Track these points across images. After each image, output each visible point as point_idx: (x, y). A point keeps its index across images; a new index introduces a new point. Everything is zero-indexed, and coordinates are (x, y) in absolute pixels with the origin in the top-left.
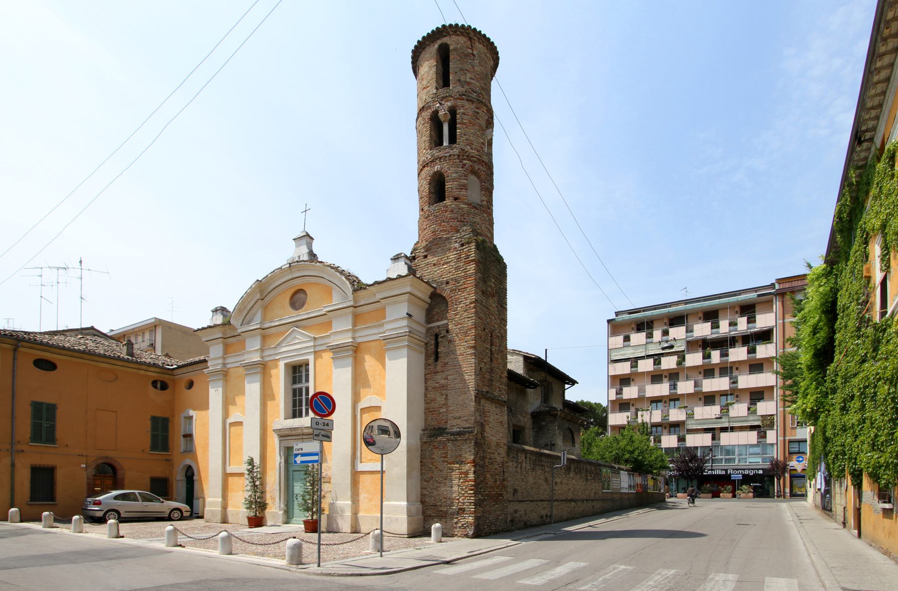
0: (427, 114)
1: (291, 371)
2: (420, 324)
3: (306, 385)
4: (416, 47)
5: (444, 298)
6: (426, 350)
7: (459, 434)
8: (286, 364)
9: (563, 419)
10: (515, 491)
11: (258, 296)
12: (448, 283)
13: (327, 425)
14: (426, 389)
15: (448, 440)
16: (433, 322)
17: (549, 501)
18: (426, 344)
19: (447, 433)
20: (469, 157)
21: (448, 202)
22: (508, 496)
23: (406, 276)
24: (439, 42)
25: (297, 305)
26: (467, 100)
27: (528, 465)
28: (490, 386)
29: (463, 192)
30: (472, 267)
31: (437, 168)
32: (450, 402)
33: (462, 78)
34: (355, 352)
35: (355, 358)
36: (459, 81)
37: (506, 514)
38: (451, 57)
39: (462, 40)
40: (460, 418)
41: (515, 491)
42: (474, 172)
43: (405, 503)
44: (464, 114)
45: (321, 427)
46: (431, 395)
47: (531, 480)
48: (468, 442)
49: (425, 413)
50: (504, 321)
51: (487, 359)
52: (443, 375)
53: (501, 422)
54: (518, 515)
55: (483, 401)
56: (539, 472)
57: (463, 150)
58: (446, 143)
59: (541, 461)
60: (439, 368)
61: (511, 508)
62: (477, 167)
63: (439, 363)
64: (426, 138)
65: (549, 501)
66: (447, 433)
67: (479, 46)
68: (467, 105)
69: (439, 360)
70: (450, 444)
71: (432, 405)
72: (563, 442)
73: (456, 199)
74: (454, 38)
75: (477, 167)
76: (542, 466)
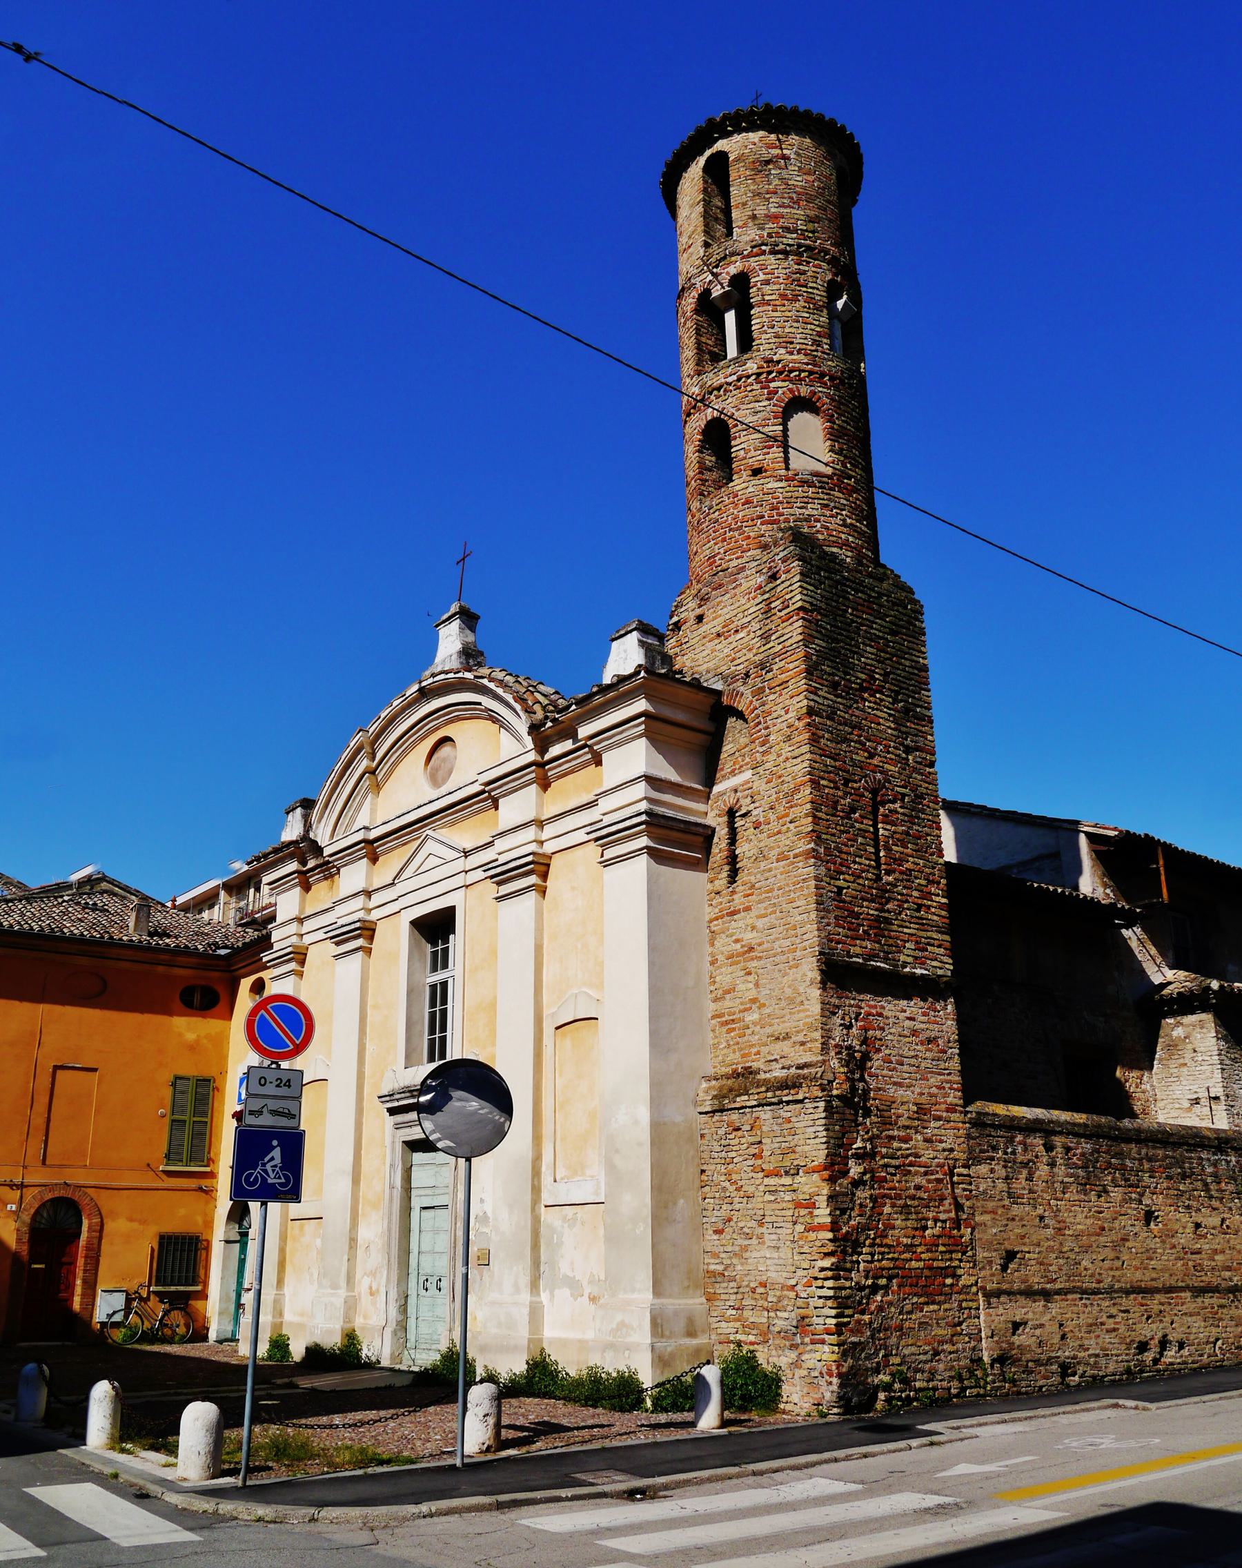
7: (785, 1085)
13: (288, 1084)
21: (741, 483)
24: (708, 153)
30: (794, 630)
38: (733, 174)
40: (787, 1037)
44: (767, 282)
45: (270, 1089)
57: (769, 361)
58: (732, 349)
63: (739, 887)
69: (742, 877)
70: (765, 1114)
73: (757, 472)
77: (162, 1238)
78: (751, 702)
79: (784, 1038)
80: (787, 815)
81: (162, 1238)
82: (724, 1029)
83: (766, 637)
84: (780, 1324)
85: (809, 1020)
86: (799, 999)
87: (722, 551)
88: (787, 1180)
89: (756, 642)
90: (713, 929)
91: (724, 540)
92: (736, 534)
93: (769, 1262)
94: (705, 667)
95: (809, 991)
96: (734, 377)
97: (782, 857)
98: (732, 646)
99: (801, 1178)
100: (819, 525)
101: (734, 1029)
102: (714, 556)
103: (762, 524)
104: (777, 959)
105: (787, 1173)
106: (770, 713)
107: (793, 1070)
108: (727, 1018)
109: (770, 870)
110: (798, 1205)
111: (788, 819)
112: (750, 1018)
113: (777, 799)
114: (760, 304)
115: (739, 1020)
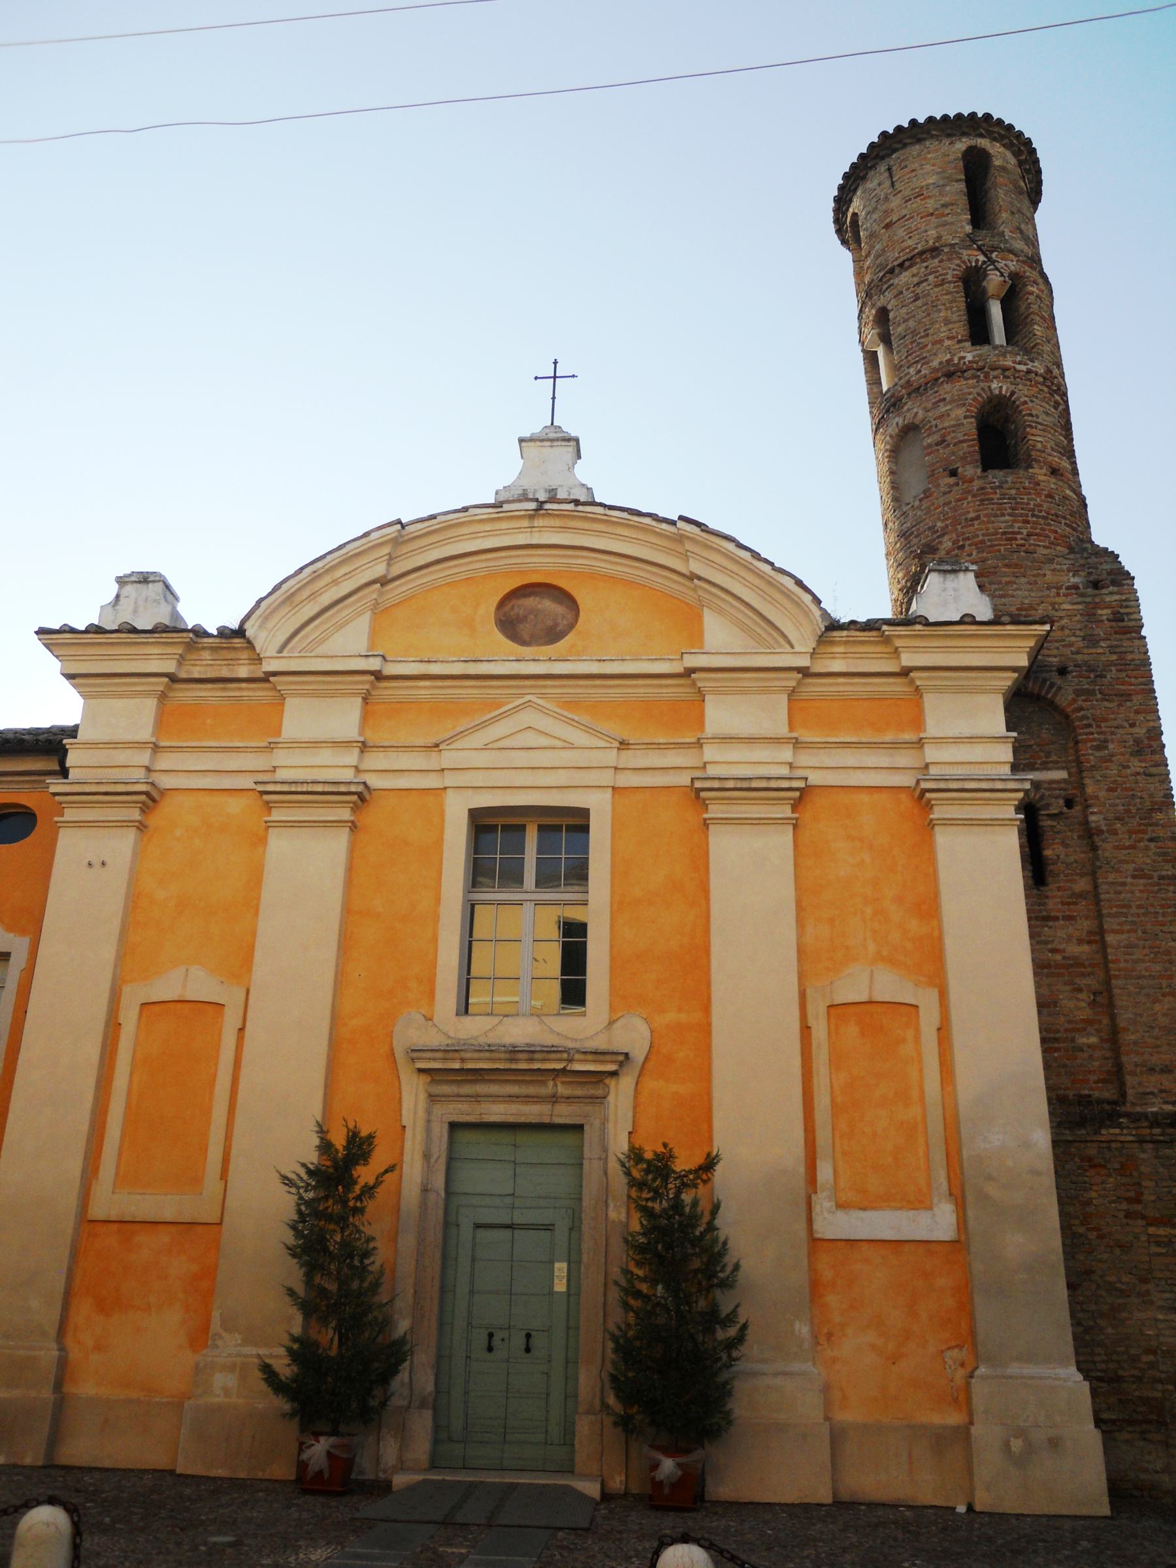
12: (1063, 671)
15: (1141, 1141)
25: (525, 629)
70: (1146, 1155)
77: (471, 811)
78: (1074, 701)
79: (1162, 1071)
81: (471, 811)
87: (1025, 532)
93: (1161, 1326)
97: (1139, 874)
101: (1057, 1050)
104: (1144, 982)
109: (1124, 884)
111: (1146, 837)
112: (1085, 1040)
113: (1128, 811)
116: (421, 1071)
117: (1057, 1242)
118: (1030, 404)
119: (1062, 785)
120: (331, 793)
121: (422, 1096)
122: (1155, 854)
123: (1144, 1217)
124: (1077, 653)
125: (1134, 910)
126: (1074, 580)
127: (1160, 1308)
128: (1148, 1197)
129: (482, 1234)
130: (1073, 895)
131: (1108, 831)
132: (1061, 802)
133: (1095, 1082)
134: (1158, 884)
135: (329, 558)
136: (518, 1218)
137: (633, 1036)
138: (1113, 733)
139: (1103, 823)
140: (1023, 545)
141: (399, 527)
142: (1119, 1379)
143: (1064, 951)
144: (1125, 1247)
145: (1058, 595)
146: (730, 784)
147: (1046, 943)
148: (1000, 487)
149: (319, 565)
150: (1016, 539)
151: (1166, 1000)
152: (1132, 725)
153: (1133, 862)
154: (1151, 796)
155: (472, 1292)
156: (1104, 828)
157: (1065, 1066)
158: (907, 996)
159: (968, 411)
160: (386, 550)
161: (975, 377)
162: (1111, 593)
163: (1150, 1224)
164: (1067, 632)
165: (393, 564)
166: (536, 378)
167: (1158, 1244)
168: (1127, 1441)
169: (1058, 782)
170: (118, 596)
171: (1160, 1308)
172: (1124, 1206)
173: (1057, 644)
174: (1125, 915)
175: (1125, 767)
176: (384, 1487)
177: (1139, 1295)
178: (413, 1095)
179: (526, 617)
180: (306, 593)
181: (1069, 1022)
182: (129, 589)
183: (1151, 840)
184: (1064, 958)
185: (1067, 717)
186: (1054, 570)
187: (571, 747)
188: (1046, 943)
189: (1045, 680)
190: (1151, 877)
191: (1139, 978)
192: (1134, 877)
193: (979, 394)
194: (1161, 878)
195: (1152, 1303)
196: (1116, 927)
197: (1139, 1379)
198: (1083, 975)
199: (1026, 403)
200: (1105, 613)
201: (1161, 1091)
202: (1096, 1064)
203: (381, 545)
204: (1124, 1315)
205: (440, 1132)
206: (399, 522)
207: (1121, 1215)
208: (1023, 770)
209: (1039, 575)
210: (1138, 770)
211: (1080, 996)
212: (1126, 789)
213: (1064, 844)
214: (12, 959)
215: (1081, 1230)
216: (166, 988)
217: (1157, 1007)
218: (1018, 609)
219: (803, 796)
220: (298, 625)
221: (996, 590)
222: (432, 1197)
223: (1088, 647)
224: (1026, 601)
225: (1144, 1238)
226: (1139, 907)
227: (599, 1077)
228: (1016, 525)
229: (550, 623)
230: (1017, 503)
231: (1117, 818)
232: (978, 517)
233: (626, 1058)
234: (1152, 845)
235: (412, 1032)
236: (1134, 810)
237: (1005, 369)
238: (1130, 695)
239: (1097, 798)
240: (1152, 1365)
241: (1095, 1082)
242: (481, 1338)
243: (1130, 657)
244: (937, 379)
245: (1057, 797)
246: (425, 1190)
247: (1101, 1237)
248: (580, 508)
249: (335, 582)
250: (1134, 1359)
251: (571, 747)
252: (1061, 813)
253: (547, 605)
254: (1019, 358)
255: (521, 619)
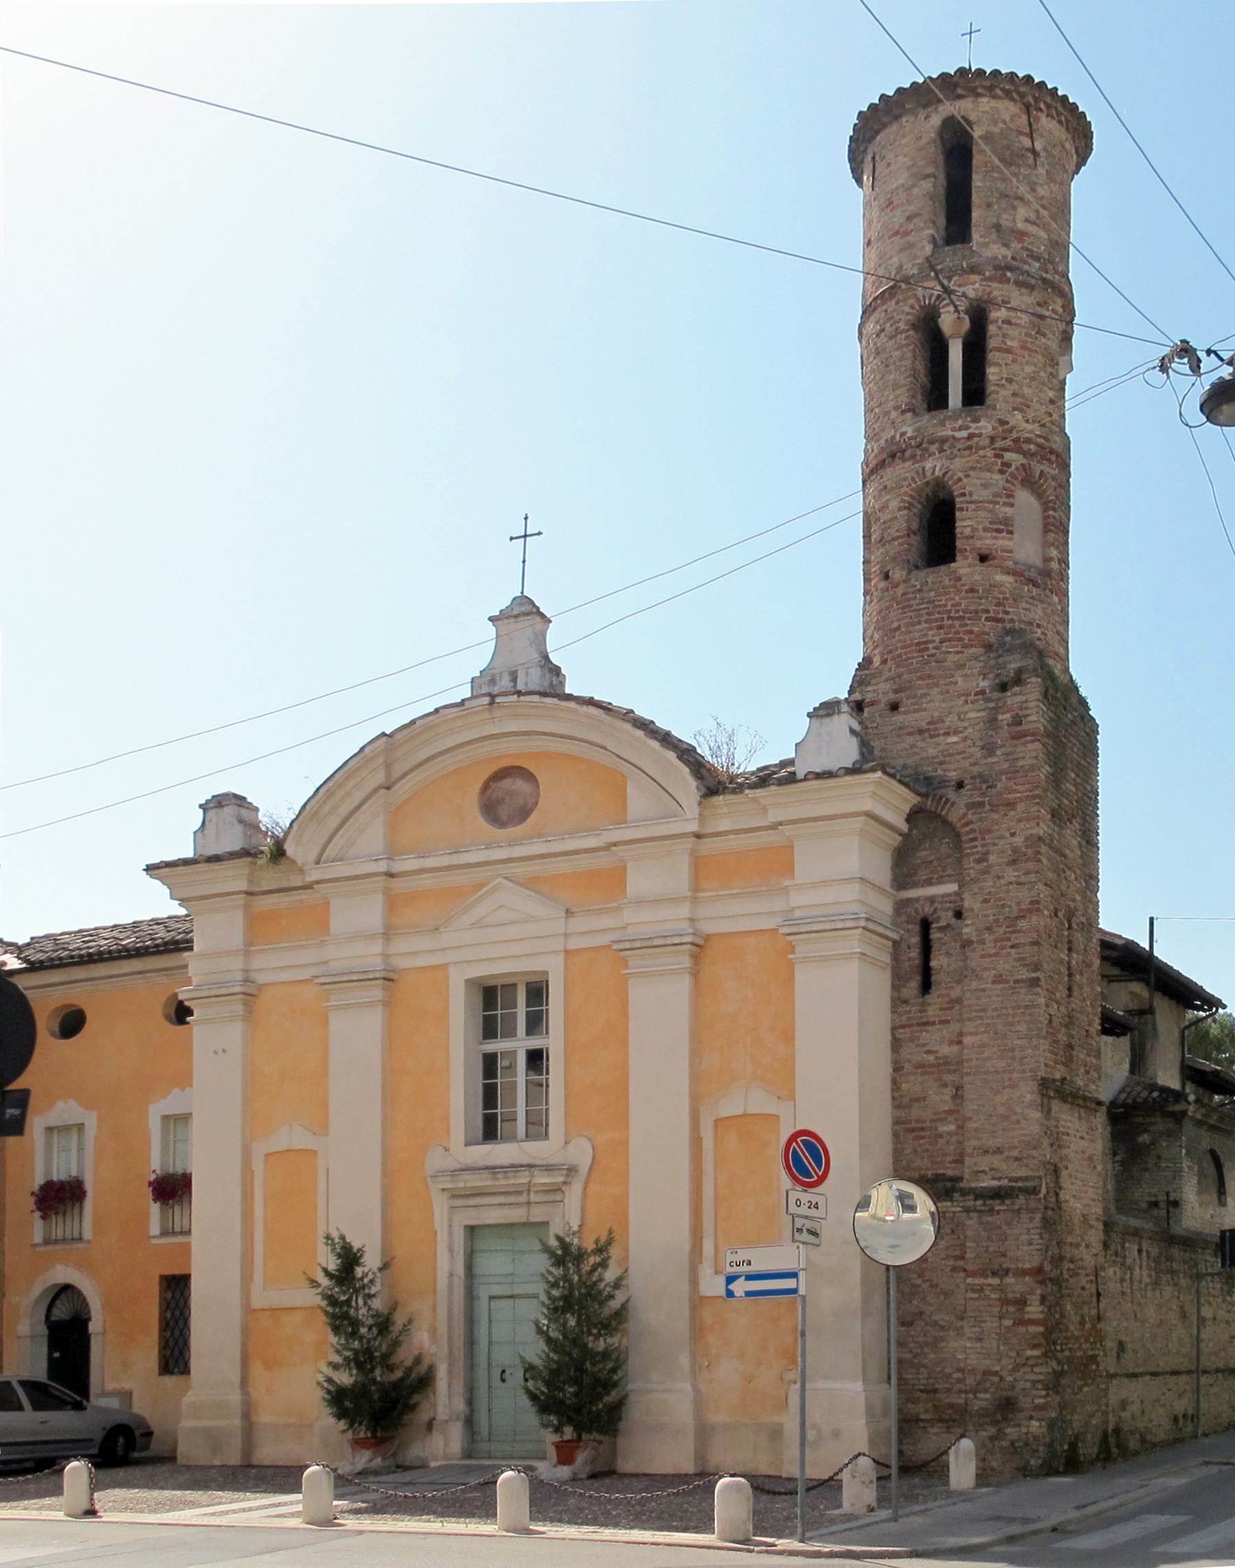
0: (905, 311)
1: (479, 1000)
2: (881, 890)
3: (535, 1043)
4: (872, 106)
5: (951, 826)
6: (895, 957)
7: (998, 1194)
8: (470, 982)
9: (1199, 1123)
10: (1121, 1346)
11: (379, 778)
12: (960, 785)
14: (897, 1068)
15: (967, 1210)
16: (915, 885)
17: (1189, 1372)
18: (896, 944)
19: (964, 1192)
20: (1018, 445)
21: (964, 566)
22: (1108, 1363)
23: (854, 770)
25: (503, 811)
26: (1019, 284)
27: (1145, 1273)
28: (1068, 1062)
29: (1003, 542)
31: (934, 465)
32: (969, 1108)
33: (1005, 222)
34: (696, 958)
35: (695, 974)
36: (998, 227)
37: (1105, 1413)
39: (1008, 110)
40: (998, 1151)
41: (1121, 1346)
42: (1029, 482)
43: (858, 1386)
44: (1007, 322)
46: (911, 1085)
47: (1151, 1314)
48: (1024, 1216)
49: (895, 1135)
50: (1091, 879)
51: (1061, 993)
52: (948, 1032)
53: (1090, 1159)
54: (1126, 1415)
55: (1056, 1105)
56: (1168, 1291)
57: (1003, 422)
59: (1170, 1259)
60: (932, 1012)
61: (1118, 1391)
62: (1037, 468)
63: (933, 997)
64: (900, 376)
65: (1189, 1372)
66: (964, 1192)
67: (1046, 123)
68: (1020, 298)
70: (972, 1222)
71: (915, 1112)
72: (1199, 1193)
73: (983, 559)
74: (986, 103)
75: (1037, 468)
76: (1173, 1273)
78: (965, 815)
79: (994, 1153)
80: (1009, 939)
82: (911, 1136)
83: (989, 749)
84: (977, 1405)
85: (1026, 1138)
86: (1014, 1118)
87: (937, 639)
88: (995, 1281)
89: (976, 752)
90: (898, 1036)
91: (940, 627)
92: (957, 623)
94: (902, 761)
95: (1026, 1111)
96: (964, 434)
97: (999, 979)
98: (940, 748)
99: (1010, 1280)
100: (1039, 631)
101: (923, 1137)
102: (926, 643)
103: (987, 619)
105: (994, 1274)
106: (989, 831)
107: (1005, 1182)
108: (914, 1125)
109: (984, 990)
110: (1005, 1302)
111: (1009, 944)
113: (996, 921)
114: (999, 350)
115: (930, 1129)
116: (443, 1190)
117: (857, 1294)
118: (965, 480)
119: (953, 898)
120: (365, 979)
121: (446, 1209)
122: (1015, 960)
123: (965, 1270)
124: (975, 764)
125: (990, 1013)
126: (984, 684)
127: (969, 1338)
128: (969, 1255)
129: (495, 1304)
130: (951, 1001)
131: (978, 942)
132: (950, 913)
133: (951, 1163)
134: (1013, 988)
135: (337, 776)
136: (518, 1290)
137: (581, 1153)
138: (995, 844)
139: (974, 934)
140: (933, 655)
141: (384, 739)
142: (935, 1391)
143: (937, 1052)
144: (946, 1294)
145: (966, 702)
146: (638, 944)
147: (924, 1045)
148: (920, 591)
149: (330, 784)
150: (927, 649)
151: (1006, 1091)
152: (1013, 835)
153: (995, 969)
154: (1018, 904)
155: (490, 1343)
156: (974, 939)
157: (927, 1150)
158: (771, 1110)
159: (903, 501)
160: (381, 760)
161: (913, 457)
162: (1015, 694)
163: (968, 1276)
164: (969, 742)
165: (386, 769)
166: (512, 539)
167: (973, 1291)
168: (936, 1434)
169: (949, 895)
170: (203, 823)
171: (969, 1338)
172: (951, 1262)
173: (958, 757)
174: (980, 1018)
175: (999, 878)
176: (423, 1466)
177: (956, 1329)
178: (440, 1207)
179: (503, 799)
180: (327, 808)
181: (934, 1113)
182: (211, 814)
183: (1012, 947)
184: (936, 1058)
185: (958, 835)
186: (966, 675)
187: (532, 919)
188: (924, 1045)
189: (941, 797)
190: (1007, 982)
191: (986, 1073)
192: (993, 982)
193: (913, 479)
194: (1016, 982)
195: (964, 1334)
196: (972, 1030)
197: (949, 1390)
198: (949, 1072)
199: (960, 479)
200: (1005, 717)
201: (991, 1169)
202: (952, 1147)
203: (374, 758)
204: (944, 1344)
205: (459, 1235)
206: (384, 734)
207: (948, 1269)
208: (923, 886)
209: (951, 683)
210: (1013, 879)
211: (945, 1090)
212: (1000, 899)
213: (948, 954)
214: (195, 1121)
215: (918, 1282)
216: (280, 1141)
217: (998, 1098)
218: (929, 723)
219: (700, 948)
220: (327, 835)
221: (912, 704)
222: (455, 1279)
223: (985, 757)
224: (936, 714)
225: (962, 1287)
226: (996, 1010)
227: (557, 1189)
228: (931, 633)
229: (521, 802)
230: (936, 607)
231: (988, 929)
232: (898, 628)
233: (572, 1170)
234: (1013, 951)
235: (436, 1160)
236: (1001, 918)
237: (943, 441)
238: (1015, 804)
239: (972, 910)
240: (959, 1381)
241: (951, 1163)
242: (496, 1373)
243: (1021, 763)
244: (884, 461)
245: (947, 910)
246: (451, 1275)
247: (932, 1286)
248: (522, 698)
249: (349, 794)
250: (949, 1376)
251: (532, 919)
252: (949, 925)
253: (519, 785)
254: (960, 422)
255: (500, 801)
